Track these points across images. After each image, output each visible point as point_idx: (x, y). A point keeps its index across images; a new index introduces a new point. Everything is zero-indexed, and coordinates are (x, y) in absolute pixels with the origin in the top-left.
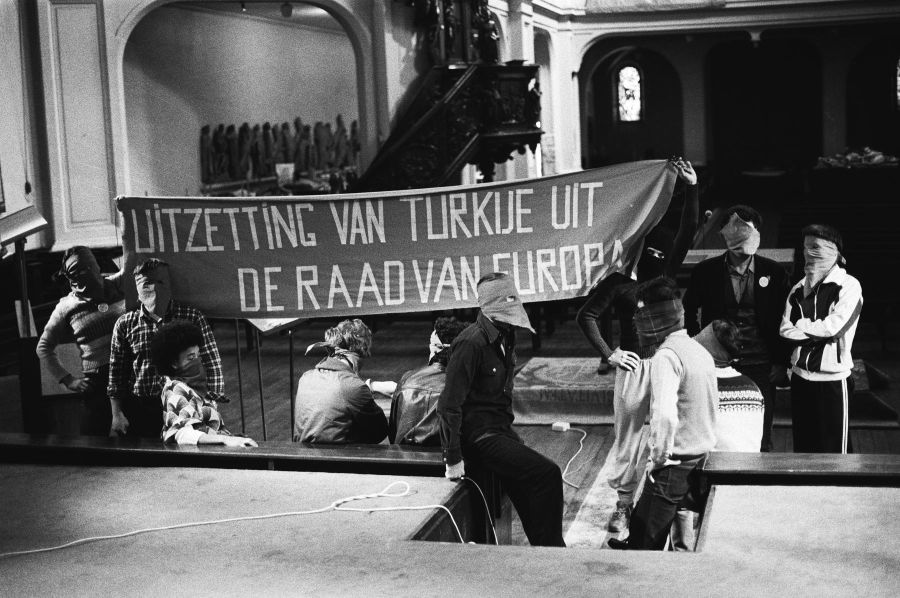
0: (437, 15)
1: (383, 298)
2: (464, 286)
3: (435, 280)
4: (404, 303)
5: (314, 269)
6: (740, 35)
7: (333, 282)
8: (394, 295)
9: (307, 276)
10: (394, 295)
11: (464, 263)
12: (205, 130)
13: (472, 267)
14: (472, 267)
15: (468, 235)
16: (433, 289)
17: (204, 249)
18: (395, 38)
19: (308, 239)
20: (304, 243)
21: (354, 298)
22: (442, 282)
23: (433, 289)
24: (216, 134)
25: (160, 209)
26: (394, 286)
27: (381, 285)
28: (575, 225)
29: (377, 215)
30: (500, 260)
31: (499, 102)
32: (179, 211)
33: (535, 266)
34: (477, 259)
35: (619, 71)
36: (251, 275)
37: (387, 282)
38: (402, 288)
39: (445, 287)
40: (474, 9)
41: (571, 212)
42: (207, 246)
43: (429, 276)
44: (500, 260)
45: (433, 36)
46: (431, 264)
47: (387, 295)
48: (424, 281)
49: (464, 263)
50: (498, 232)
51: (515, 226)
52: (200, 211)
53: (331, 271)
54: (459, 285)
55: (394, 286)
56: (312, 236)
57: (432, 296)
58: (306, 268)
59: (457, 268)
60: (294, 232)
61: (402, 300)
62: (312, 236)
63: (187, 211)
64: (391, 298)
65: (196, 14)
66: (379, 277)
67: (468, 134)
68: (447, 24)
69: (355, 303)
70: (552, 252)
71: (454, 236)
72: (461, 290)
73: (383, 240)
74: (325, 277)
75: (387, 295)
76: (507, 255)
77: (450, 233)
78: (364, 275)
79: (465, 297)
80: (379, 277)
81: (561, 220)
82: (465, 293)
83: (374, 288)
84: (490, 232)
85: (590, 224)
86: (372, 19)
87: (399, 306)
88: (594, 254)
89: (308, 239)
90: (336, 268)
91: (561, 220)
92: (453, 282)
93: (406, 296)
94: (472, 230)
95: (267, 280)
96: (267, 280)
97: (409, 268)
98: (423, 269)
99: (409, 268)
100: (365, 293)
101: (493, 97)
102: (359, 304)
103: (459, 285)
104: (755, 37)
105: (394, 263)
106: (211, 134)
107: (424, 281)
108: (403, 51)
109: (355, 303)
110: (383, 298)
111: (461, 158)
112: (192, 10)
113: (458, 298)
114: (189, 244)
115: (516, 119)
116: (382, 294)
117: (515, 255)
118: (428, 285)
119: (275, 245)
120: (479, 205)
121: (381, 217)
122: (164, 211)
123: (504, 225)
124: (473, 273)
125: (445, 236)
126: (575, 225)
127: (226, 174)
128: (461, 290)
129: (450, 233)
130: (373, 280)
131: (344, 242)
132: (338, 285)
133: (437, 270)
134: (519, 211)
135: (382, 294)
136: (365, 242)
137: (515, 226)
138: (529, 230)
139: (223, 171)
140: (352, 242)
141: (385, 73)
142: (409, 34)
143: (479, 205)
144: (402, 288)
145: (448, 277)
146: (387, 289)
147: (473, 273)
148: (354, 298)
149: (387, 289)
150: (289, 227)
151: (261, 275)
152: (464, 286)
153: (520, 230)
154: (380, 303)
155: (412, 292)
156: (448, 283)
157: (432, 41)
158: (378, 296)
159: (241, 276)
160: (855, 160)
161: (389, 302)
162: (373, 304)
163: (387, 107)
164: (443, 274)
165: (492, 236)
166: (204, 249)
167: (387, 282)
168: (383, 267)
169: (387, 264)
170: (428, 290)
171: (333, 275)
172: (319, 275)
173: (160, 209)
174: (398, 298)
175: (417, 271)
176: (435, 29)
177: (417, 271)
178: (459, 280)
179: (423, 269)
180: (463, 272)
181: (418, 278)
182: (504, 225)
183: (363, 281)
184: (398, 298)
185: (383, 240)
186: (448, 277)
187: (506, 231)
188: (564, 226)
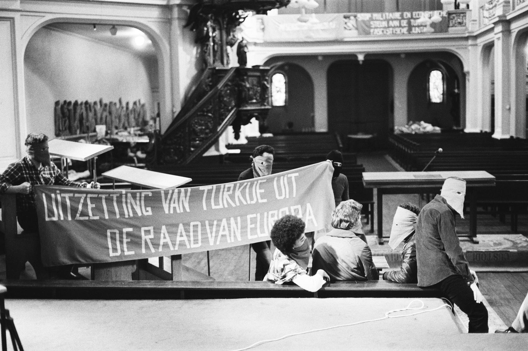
0: (210, 37)
1: (190, 243)
2: (232, 234)
3: (217, 232)
4: (201, 246)
5: (151, 228)
6: (353, 56)
7: (162, 235)
8: (196, 241)
9: (147, 232)
10: (196, 241)
11: (232, 221)
12: (57, 103)
13: (236, 223)
14: (236, 223)
15: (233, 205)
16: (216, 237)
17: (87, 218)
18: (185, 50)
19: (147, 211)
20: (145, 214)
21: (174, 245)
22: (221, 233)
23: (216, 237)
24: (62, 107)
25: (60, 194)
26: (195, 236)
27: (188, 236)
28: (287, 197)
29: (186, 197)
30: (251, 218)
31: (249, 89)
32: (72, 195)
33: (267, 220)
34: (239, 219)
35: (272, 76)
36: (115, 233)
37: (192, 234)
38: (200, 237)
39: (222, 236)
40: (228, 34)
41: (285, 188)
42: (89, 216)
43: (214, 229)
44: (251, 218)
45: (207, 49)
46: (215, 223)
47: (192, 242)
48: (211, 233)
49: (232, 221)
50: (249, 202)
51: (257, 199)
52: (85, 195)
53: (161, 229)
54: (230, 234)
55: (195, 236)
56: (149, 209)
57: (215, 242)
58: (146, 228)
59: (229, 224)
60: (139, 207)
61: (200, 244)
62: (149, 209)
63: (77, 195)
64: (194, 243)
65: (53, 32)
66: (187, 231)
67: (230, 108)
68: (214, 41)
69: (174, 247)
70: (276, 212)
71: (226, 206)
72: (230, 236)
73: (188, 210)
74: (157, 231)
75: (192, 242)
76: (254, 215)
77: (223, 205)
78: (179, 231)
79: (233, 241)
80: (187, 231)
81: (280, 195)
82: (232, 238)
83: (185, 238)
84: (245, 203)
85: (294, 196)
86: (170, 35)
87: (197, 248)
88: (297, 211)
89: (147, 211)
90: (164, 227)
91: (280, 195)
92: (227, 233)
93: (202, 242)
94: (234, 202)
95: (124, 236)
96: (124, 236)
97: (203, 225)
98: (211, 225)
99: (203, 225)
100: (180, 241)
101: (245, 86)
102: (176, 248)
103: (230, 234)
104: (361, 58)
105: (195, 223)
106: (60, 106)
107: (211, 233)
108: (188, 58)
109: (174, 247)
110: (190, 243)
111: (226, 123)
112: (51, 29)
113: (229, 241)
114: (78, 215)
115: (256, 99)
116: (189, 241)
117: (259, 215)
118: (214, 234)
119: (129, 215)
120: (239, 189)
121: (188, 198)
122: (63, 195)
123: (251, 199)
124: (237, 226)
125: (221, 206)
126: (287, 197)
127: (68, 131)
128: (230, 236)
129: (223, 205)
130: (184, 233)
131: (167, 211)
132: (165, 238)
133: (218, 226)
134: (258, 191)
135: (189, 241)
136: (178, 211)
137: (257, 199)
138: (265, 201)
139: (66, 129)
140: (172, 212)
141: (178, 70)
142: (192, 46)
143: (239, 189)
144: (200, 237)
145: (224, 230)
146: (192, 238)
147: (237, 226)
148: (174, 245)
149: (192, 238)
150: (136, 204)
151: (121, 233)
152: (232, 234)
153: (260, 201)
154: (188, 247)
155: (205, 240)
156: (224, 233)
157: (206, 52)
158: (187, 243)
159: (109, 234)
160: (417, 129)
161: (193, 246)
162: (185, 247)
163: (178, 93)
164: (222, 228)
165: (246, 205)
166: (87, 218)
167: (192, 234)
168: (189, 226)
169: (192, 224)
170: (213, 238)
171: (162, 231)
172: (154, 232)
173: (60, 194)
174: (197, 243)
175: (208, 227)
176: (207, 45)
177: (208, 227)
178: (230, 231)
179: (211, 225)
180: (232, 226)
181: (208, 231)
182: (251, 199)
183: (179, 234)
184: (197, 243)
185: (188, 210)
186: (224, 230)
187: (253, 202)
188: (282, 197)
